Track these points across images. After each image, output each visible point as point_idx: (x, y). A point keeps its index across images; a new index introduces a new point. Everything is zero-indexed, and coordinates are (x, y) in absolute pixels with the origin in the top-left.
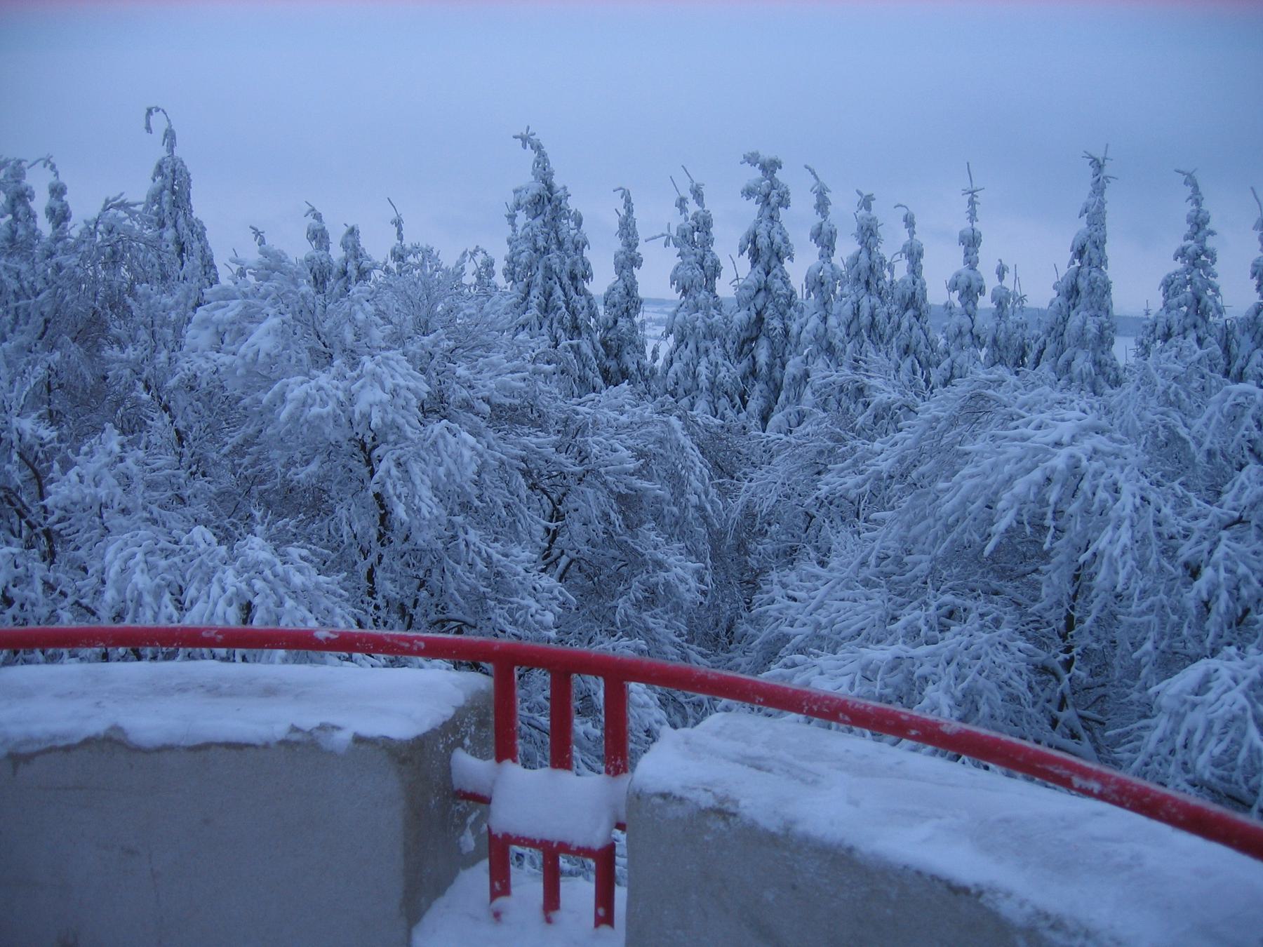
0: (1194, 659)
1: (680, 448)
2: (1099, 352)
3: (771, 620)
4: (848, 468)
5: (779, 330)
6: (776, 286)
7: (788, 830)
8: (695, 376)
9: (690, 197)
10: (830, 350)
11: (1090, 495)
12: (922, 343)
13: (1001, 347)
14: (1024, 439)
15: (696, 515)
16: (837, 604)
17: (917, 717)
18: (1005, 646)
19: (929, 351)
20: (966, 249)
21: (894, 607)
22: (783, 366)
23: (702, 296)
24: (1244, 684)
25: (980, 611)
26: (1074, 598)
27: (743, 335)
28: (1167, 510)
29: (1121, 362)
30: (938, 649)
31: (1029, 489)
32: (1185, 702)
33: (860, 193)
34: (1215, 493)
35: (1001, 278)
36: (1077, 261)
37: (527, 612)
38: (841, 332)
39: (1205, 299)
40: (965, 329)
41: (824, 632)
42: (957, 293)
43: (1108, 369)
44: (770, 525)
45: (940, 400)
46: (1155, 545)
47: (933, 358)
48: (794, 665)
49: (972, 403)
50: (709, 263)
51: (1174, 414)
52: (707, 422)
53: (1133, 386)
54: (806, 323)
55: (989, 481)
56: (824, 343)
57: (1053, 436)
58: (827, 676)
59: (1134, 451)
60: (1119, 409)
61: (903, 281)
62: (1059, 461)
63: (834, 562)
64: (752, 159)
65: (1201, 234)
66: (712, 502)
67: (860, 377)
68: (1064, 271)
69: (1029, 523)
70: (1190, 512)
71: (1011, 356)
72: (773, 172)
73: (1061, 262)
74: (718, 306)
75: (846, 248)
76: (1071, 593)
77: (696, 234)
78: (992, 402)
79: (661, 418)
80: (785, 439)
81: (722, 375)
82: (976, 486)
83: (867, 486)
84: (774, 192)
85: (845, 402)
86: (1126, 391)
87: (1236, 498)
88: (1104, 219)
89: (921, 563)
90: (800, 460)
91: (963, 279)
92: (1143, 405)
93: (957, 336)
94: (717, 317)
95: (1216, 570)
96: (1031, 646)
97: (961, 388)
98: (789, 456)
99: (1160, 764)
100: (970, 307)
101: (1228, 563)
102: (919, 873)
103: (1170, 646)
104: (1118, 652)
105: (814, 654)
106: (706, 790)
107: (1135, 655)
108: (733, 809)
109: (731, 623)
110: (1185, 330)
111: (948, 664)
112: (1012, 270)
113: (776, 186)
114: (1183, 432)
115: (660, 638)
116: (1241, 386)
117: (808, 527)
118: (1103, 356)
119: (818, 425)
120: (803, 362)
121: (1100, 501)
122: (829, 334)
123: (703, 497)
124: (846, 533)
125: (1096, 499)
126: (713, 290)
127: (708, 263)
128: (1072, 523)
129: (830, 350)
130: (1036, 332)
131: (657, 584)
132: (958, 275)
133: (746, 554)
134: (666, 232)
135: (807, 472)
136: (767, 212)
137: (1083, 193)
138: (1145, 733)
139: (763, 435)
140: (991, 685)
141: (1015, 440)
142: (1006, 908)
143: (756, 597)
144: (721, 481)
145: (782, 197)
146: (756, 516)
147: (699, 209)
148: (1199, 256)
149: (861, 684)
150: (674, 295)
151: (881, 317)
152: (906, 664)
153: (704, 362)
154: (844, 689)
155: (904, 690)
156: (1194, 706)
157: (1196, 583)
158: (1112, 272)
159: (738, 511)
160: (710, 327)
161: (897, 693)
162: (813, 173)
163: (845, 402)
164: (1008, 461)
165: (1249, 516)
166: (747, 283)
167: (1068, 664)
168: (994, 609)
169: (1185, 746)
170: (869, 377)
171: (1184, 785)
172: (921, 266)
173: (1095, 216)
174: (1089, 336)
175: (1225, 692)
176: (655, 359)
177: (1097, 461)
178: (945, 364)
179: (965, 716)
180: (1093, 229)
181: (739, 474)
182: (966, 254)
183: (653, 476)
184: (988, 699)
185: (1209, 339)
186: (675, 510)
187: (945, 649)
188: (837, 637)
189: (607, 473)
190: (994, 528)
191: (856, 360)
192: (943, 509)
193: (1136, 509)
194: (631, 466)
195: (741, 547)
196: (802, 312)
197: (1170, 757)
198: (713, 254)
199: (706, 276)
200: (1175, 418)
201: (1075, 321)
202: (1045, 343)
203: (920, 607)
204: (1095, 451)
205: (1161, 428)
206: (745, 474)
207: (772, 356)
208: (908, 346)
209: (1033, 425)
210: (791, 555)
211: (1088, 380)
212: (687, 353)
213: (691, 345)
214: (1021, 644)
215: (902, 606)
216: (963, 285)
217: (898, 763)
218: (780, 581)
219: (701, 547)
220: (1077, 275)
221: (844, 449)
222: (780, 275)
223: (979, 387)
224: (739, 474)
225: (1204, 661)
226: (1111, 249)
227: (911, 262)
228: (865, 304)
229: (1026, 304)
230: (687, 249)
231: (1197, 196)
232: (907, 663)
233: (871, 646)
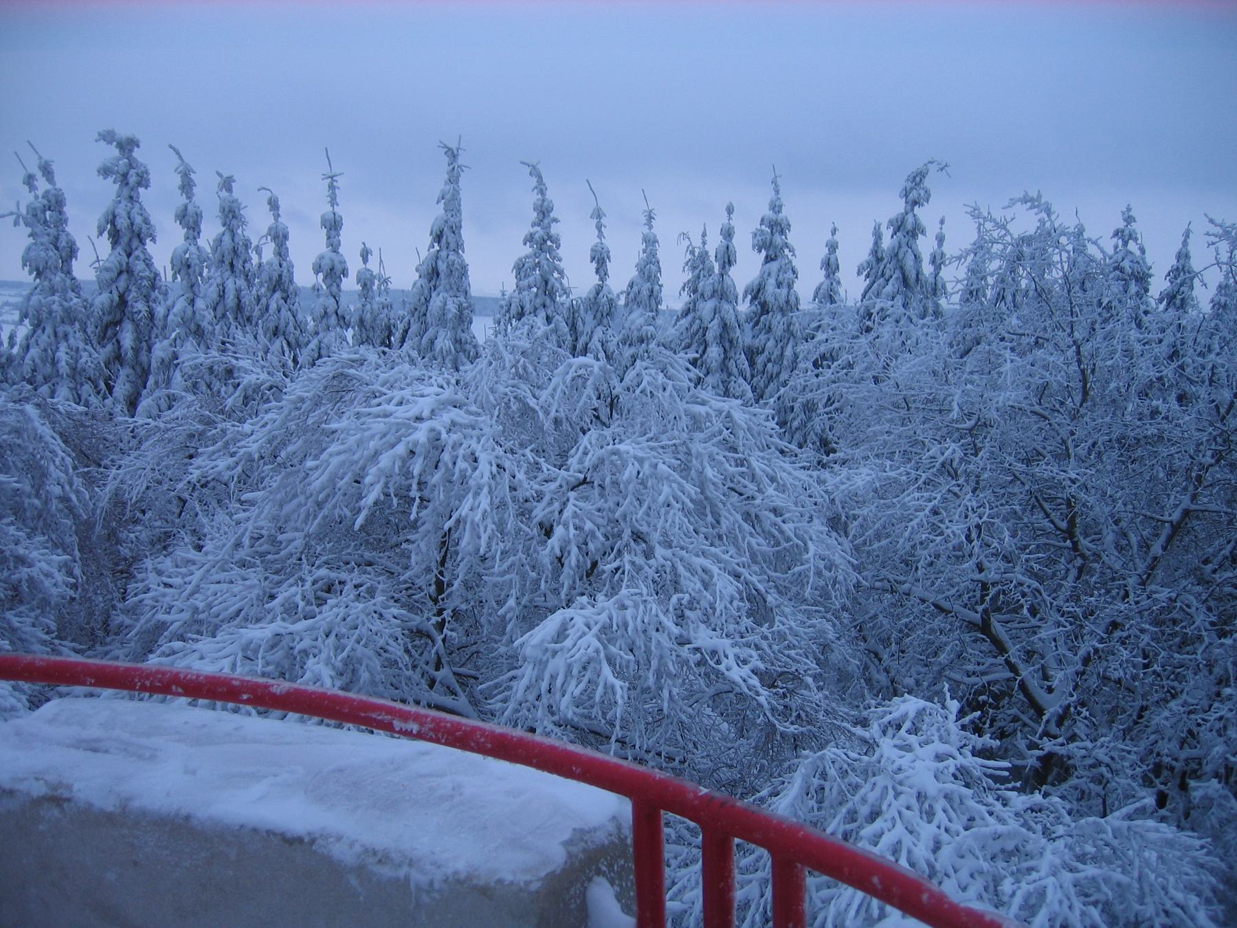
0: (552, 611)
1: (37, 438)
2: (459, 331)
3: (148, 608)
4: (219, 451)
5: (144, 313)
6: (138, 267)
7: (124, 808)
8: (54, 363)
9: (39, 174)
10: (199, 333)
11: (450, 465)
12: (291, 324)
13: (368, 327)
14: (386, 416)
15: (61, 506)
16: (213, 587)
17: (249, 681)
18: (381, 615)
19: (298, 332)
21: (271, 585)
22: (150, 350)
23: (58, 278)
24: (595, 629)
25: (354, 582)
26: (443, 563)
27: (106, 319)
28: (521, 476)
29: (481, 340)
30: (316, 623)
31: (394, 463)
32: (547, 650)
33: (219, 174)
34: (562, 460)
35: (365, 260)
36: (436, 245)
38: (209, 315)
39: (552, 280)
40: (331, 309)
41: (201, 616)
42: (321, 276)
43: (468, 347)
44: (144, 512)
45: (304, 381)
46: (512, 509)
47: (303, 340)
48: (174, 653)
49: (335, 383)
50: (64, 244)
51: (523, 386)
52: (69, 409)
53: (485, 362)
54: (172, 305)
55: (356, 457)
56: (193, 327)
57: (414, 411)
58: (207, 660)
59: (489, 422)
60: (473, 383)
61: (270, 264)
62: (421, 435)
63: (209, 546)
64: (107, 137)
65: (546, 221)
66: (77, 492)
67: (228, 359)
68: (424, 254)
69: (396, 496)
70: (541, 477)
71: (378, 335)
72: (131, 151)
73: (420, 246)
74: (76, 288)
75: (211, 231)
76: (439, 559)
77: (48, 213)
78: (355, 381)
79: (18, 406)
80: (153, 424)
81: (83, 360)
82: (344, 463)
83: (239, 469)
84: (132, 172)
85: (217, 385)
86: (479, 367)
87: (581, 462)
88: (460, 206)
89: (295, 540)
90: (170, 445)
91: (326, 261)
92: (496, 379)
93: (323, 317)
94: (75, 300)
95: (567, 529)
96: (403, 612)
97: (326, 368)
98: (158, 441)
99: (529, 710)
100: (334, 288)
101: (577, 521)
102: (255, 830)
103: (531, 601)
104: (485, 611)
105: (193, 640)
106: (37, 779)
107: (501, 612)
108: (66, 795)
109: (107, 617)
110: (536, 309)
111: (327, 636)
112: (376, 252)
113: (134, 165)
114: (532, 402)
115: (27, 637)
116: (581, 359)
117: (181, 512)
118: (463, 335)
119: (189, 408)
120: (171, 345)
121: (461, 471)
122: (198, 317)
123: (67, 487)
124: (221, 516)
125: (457, 470)
126: (69, 272)
127: (63, 243)
128: (436, 493)
129: (199, 333)
130: (401, 313)
131: (20, 581)
132: (322, 257)
133: (117, 544)
134: (14, 210)
135: (179, 455)
136: (126, 192)
137: (438, 184)
138: (513, 683)
139: (130, 420)
140: (369, 652)
141: (379, 416)
142: (338, 851)
143: (131, 587)
144: (86, 470)
145: (142, 177)
146: (126, 503)
147: (49, 187)
148: (545, 241)
149: (243, 665)
150: (27, 277)
151: (248, 298)
152: (286, 641)
153: (63, 347)
154: (227, 670)
155: (286, 666)
156: (555, 653)
157: (549, 541)
158: (468, 256)
159: (106, 500)
160: (68, 311)
161: (280, 669)
162: (178, 153)
163: (217, 385)
164: (373, 437)
165: (591, 477)
166: (108, 265)
167: (440, 626)
168: (368, 580)
169: (550, 691)
170: (237, 359)
171: (550, 727)
172: (287, 249)
173: (451, 202)
174: (450, 316)
175: (581, 637)
176: (12, 345)
177: (455, 433)
178: (313, 344)
179: (347, 684)
180: (449, 215)
181: (106, 462)
182: (329, 238)
183: (9, 468)
184: (367, 666)
185: (557, 317)
186: (36, 502)
187: (323, 622)
188: (217, 621)
190: (362, 503)
191: (223, 343)
192: (312, 487)
193: (493, 477)
195: (112, 537)
196: (166, 294)
197: (537, 703)
198: (68, 235)
199: (61, 258)
200: (524, 390)
201: (436, 302)
202: (409, 323)
203: (296, 584)
204: (454, 423)
205: (512, 399)
206: (113, 461)
207: (138, 340)
208: (277, 328)
209: (395, 401)
210: (165, 541)
211: (450, 357)
212: (44, 338)
213: (49, 330)
214: (395, 611)
215: (279, 583)
216: (326, 268)
217: (236, 729)
218: (155, 569)
219: (68, 540)
220: (437, 258)
221: (214, 431)
222: (142, 256)
223: (342, 367)
224: (106, 462)
225: (562, 610)
226: (468, 234)
227: (277, 245)
228: (230, 285)
229: (390, 285)
230: (39, 228)
231: (542, 187)
232: (287, 639)
233: (250, 626)
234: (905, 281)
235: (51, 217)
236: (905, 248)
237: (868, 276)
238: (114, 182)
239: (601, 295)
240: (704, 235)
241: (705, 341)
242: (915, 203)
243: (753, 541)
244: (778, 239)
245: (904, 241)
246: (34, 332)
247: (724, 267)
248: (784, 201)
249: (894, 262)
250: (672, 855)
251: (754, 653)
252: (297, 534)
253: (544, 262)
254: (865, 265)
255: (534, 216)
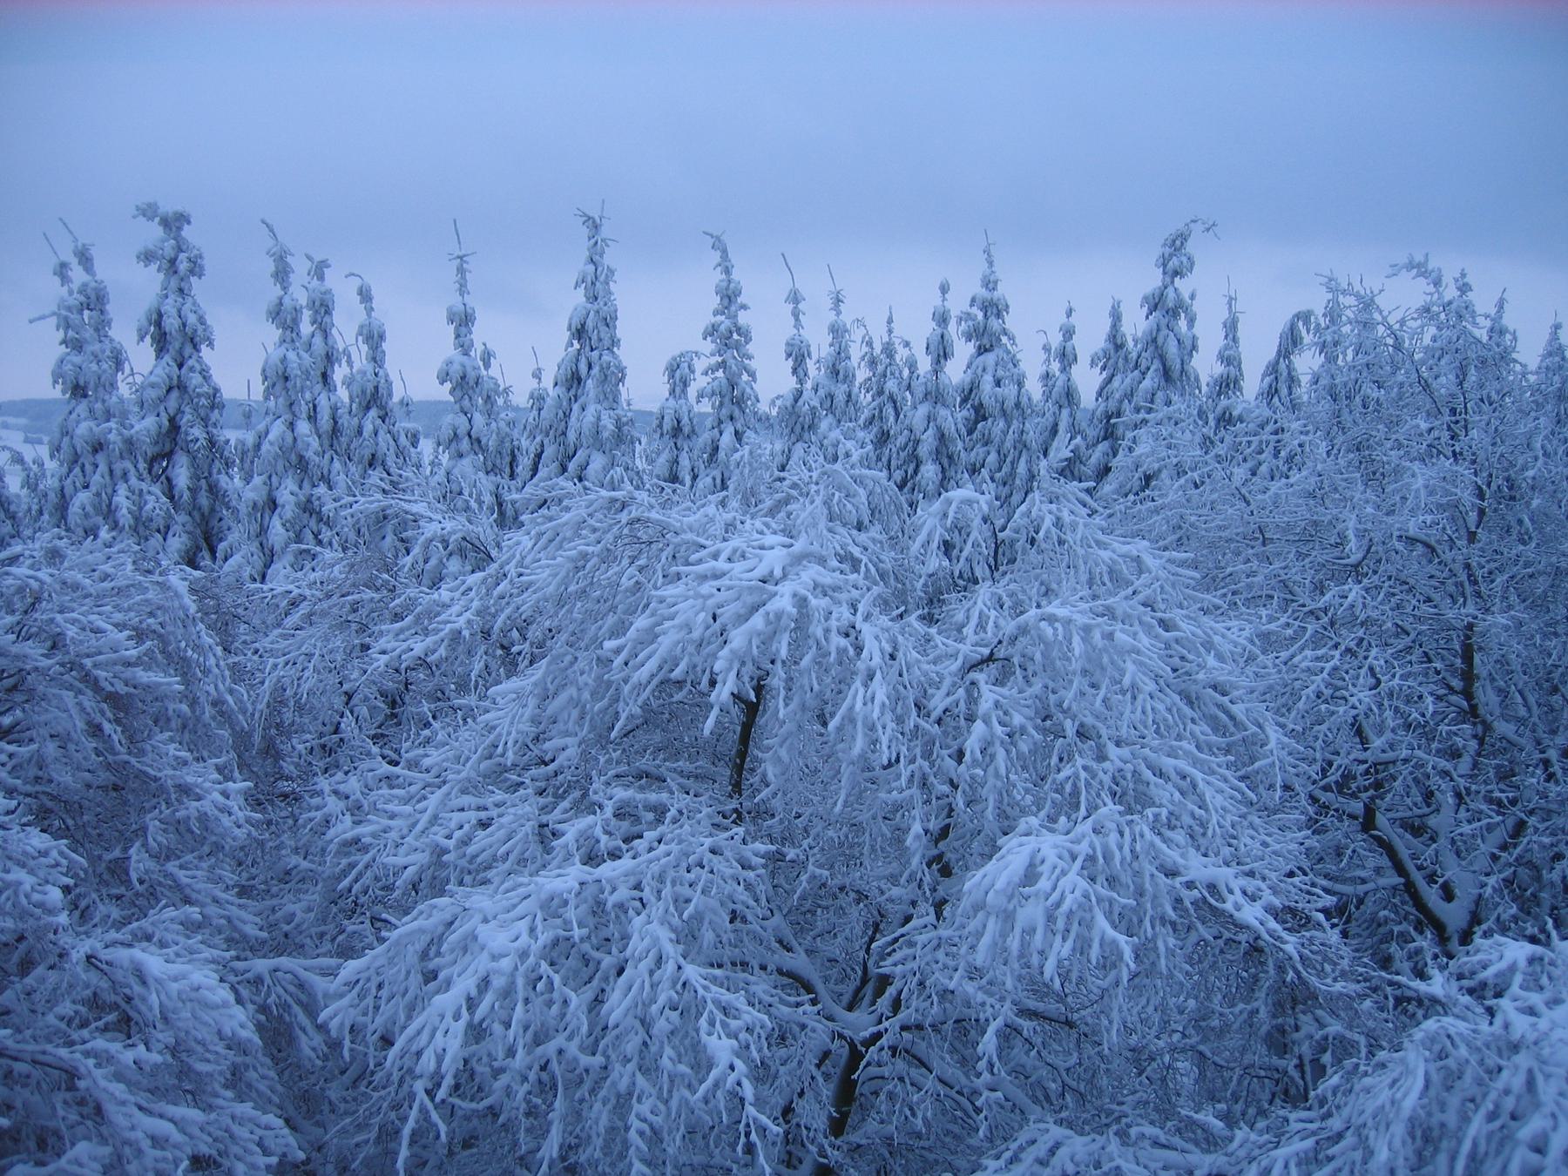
4: (408, 628)
16: (457, 816)
20: (456, 329)
37: (16, 894)
40: (462, 431)
56: (293, 458)
62: (783, 601)
72: (179, 229)
73: (555, 350)
81: (149, 507)
84: (182, 256)
91: (456, 367)
93: (451, 441)
100: (466, 402)
122: (300, 444)
132: (449, 363)
136: (174, 283)
153: (122, 490)
162: (272, 230)
166: (153, 379)
173: (596, 284)
174: (606, 434)
182: (458, 336)
189: (95, 665)
194: (134, 652)
198: (112, 340)
202: (542, 445)
207: (196, 477)
209: (723, 556)
216: (456, 376)
222: (198, 367)
227: (371, 348)
234: (1166, 373)
235: (90, 318)
236: (1165, 331)
237: (1104, 368)
238: (159, 270)
239: (800, 402)
240: (890, 321)
241: (917, 457)
242: (1176, 273)
243: (1197, 729)
244: (995, 324)
245: (1164, 322)
246: (70, 471)
247: (938, 362)
248: (999, 275)
249: (1151, 349)
250: (1161, 1165)
251: (1263, 886)
252: (569, 741)
253: (731, 362)
254: (1101, 354)
255: (715, 301)
